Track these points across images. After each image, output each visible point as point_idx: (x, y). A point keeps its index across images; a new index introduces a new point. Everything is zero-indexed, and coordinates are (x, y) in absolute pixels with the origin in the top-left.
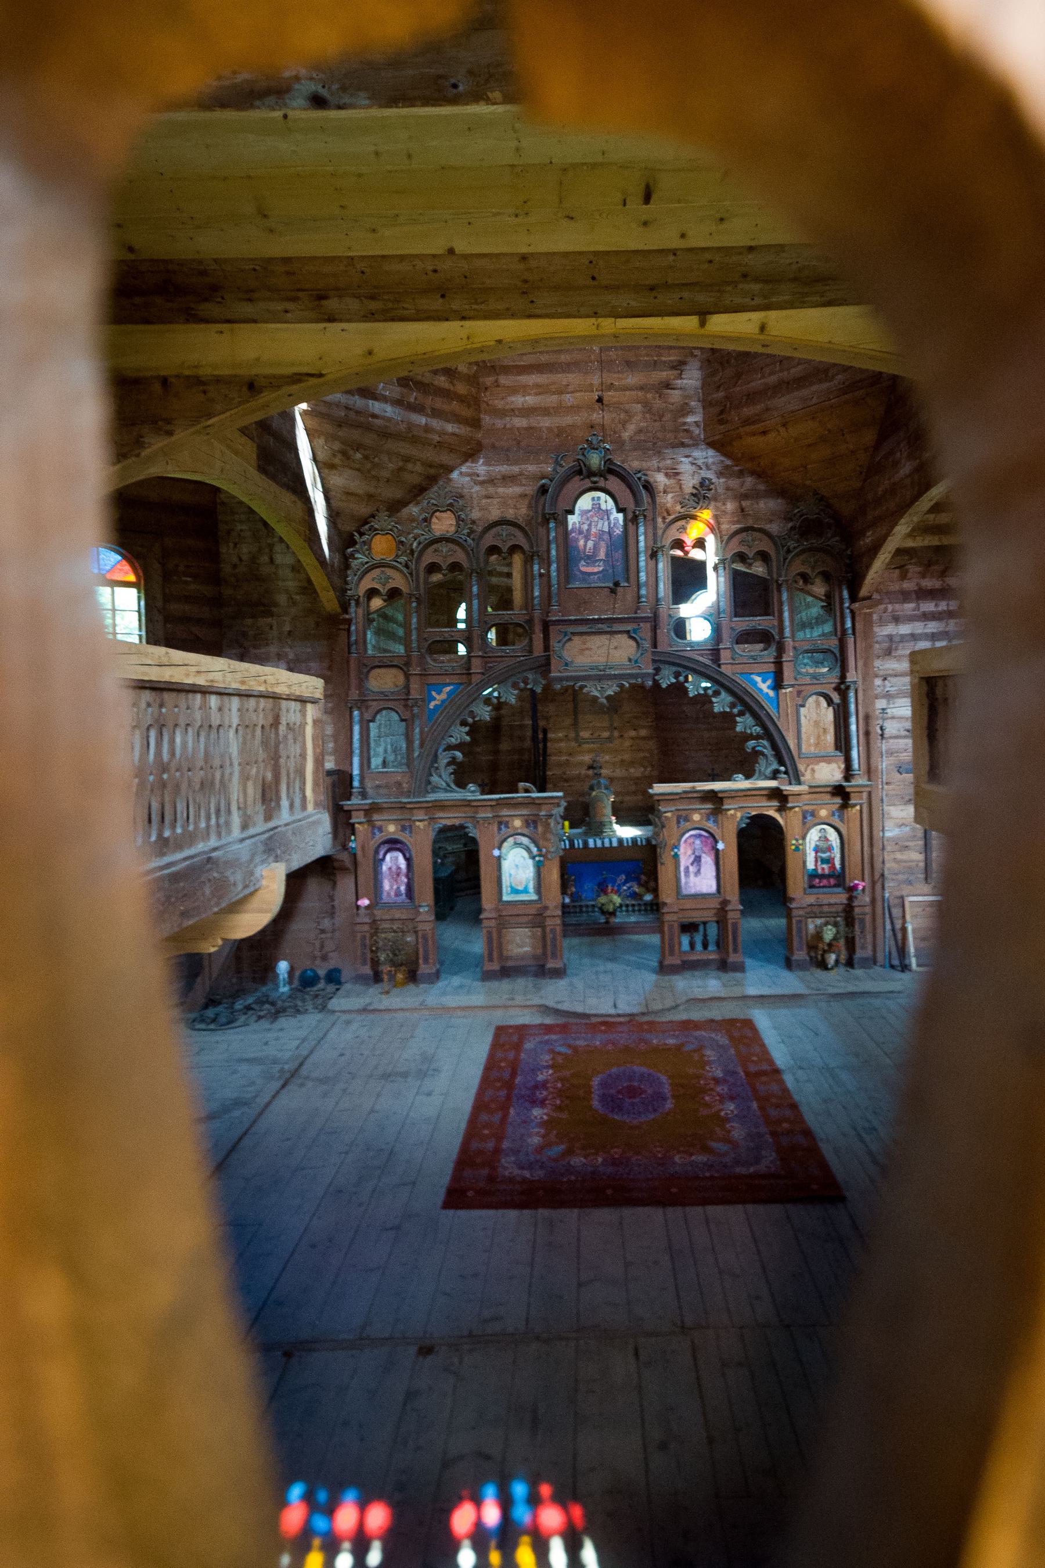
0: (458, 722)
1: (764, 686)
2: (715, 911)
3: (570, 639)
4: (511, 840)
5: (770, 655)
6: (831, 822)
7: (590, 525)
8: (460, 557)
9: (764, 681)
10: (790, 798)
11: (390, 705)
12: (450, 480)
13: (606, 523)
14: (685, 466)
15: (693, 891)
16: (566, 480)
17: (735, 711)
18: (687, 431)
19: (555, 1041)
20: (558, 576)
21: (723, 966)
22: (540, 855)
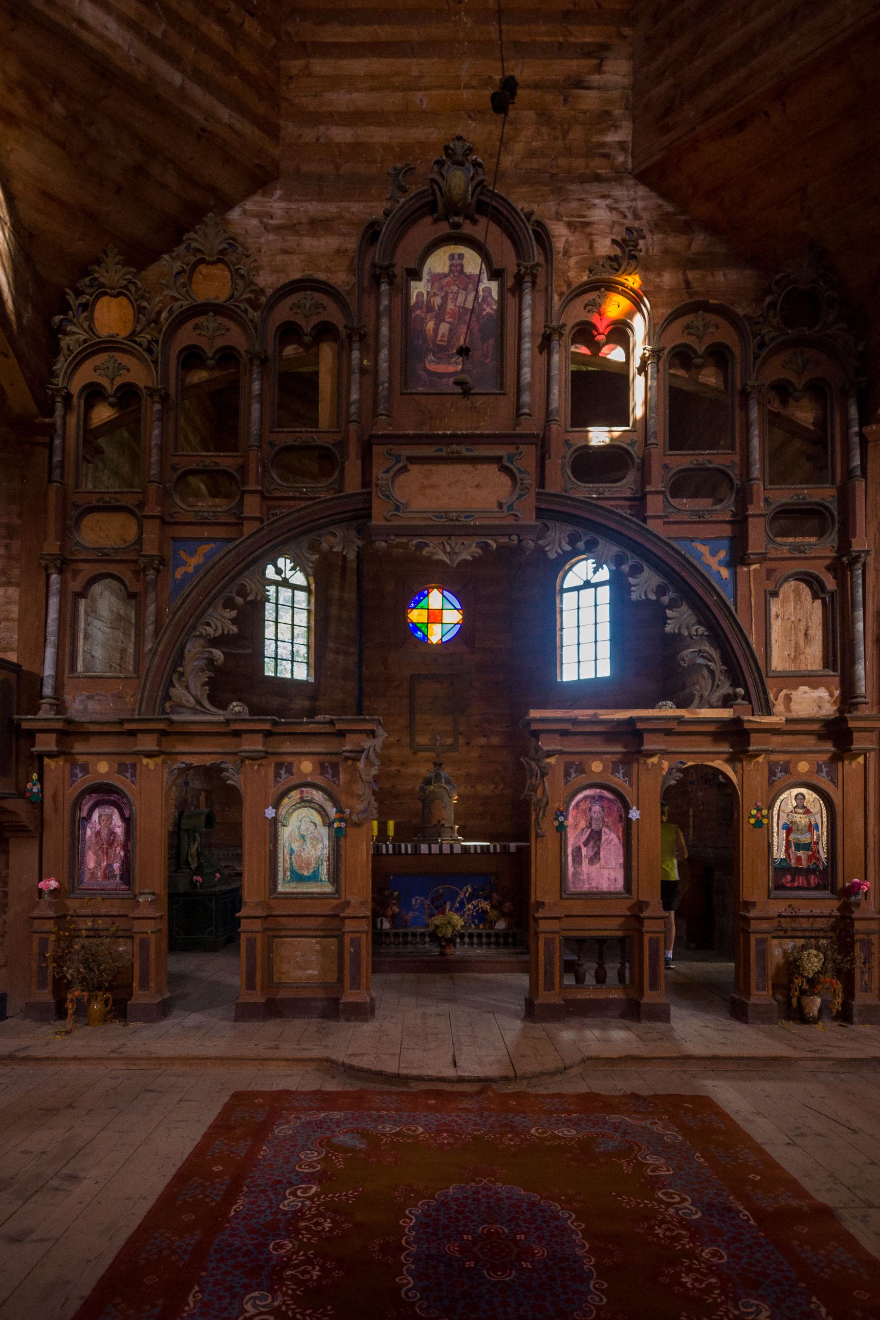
0: (220, 602)
1: (713, 561)
2: (620, 920)
3: (404, 469)
4: (295, 795)
5: (725, 510)
6: (814, 781)
7: (445, 299)
8: (236, 338)
9: (713, 553)
10: (754, 737)
11: (112, 569)
12: (227, 222)
13: (471, 297)
14: (600, 214)
15: (586, 888)
16: (409, 220)
17: (665, 599)
18: (606, 156)
19: (338, 1124)
20: (391, 369)
21: (633, 1011)
22: (341, 820)
